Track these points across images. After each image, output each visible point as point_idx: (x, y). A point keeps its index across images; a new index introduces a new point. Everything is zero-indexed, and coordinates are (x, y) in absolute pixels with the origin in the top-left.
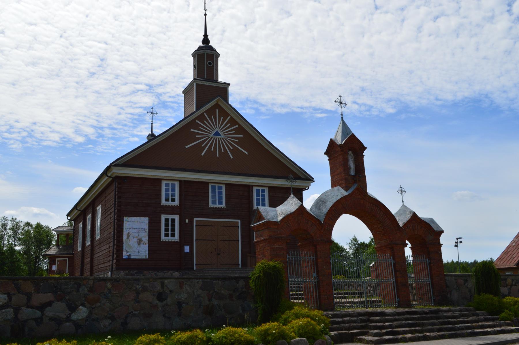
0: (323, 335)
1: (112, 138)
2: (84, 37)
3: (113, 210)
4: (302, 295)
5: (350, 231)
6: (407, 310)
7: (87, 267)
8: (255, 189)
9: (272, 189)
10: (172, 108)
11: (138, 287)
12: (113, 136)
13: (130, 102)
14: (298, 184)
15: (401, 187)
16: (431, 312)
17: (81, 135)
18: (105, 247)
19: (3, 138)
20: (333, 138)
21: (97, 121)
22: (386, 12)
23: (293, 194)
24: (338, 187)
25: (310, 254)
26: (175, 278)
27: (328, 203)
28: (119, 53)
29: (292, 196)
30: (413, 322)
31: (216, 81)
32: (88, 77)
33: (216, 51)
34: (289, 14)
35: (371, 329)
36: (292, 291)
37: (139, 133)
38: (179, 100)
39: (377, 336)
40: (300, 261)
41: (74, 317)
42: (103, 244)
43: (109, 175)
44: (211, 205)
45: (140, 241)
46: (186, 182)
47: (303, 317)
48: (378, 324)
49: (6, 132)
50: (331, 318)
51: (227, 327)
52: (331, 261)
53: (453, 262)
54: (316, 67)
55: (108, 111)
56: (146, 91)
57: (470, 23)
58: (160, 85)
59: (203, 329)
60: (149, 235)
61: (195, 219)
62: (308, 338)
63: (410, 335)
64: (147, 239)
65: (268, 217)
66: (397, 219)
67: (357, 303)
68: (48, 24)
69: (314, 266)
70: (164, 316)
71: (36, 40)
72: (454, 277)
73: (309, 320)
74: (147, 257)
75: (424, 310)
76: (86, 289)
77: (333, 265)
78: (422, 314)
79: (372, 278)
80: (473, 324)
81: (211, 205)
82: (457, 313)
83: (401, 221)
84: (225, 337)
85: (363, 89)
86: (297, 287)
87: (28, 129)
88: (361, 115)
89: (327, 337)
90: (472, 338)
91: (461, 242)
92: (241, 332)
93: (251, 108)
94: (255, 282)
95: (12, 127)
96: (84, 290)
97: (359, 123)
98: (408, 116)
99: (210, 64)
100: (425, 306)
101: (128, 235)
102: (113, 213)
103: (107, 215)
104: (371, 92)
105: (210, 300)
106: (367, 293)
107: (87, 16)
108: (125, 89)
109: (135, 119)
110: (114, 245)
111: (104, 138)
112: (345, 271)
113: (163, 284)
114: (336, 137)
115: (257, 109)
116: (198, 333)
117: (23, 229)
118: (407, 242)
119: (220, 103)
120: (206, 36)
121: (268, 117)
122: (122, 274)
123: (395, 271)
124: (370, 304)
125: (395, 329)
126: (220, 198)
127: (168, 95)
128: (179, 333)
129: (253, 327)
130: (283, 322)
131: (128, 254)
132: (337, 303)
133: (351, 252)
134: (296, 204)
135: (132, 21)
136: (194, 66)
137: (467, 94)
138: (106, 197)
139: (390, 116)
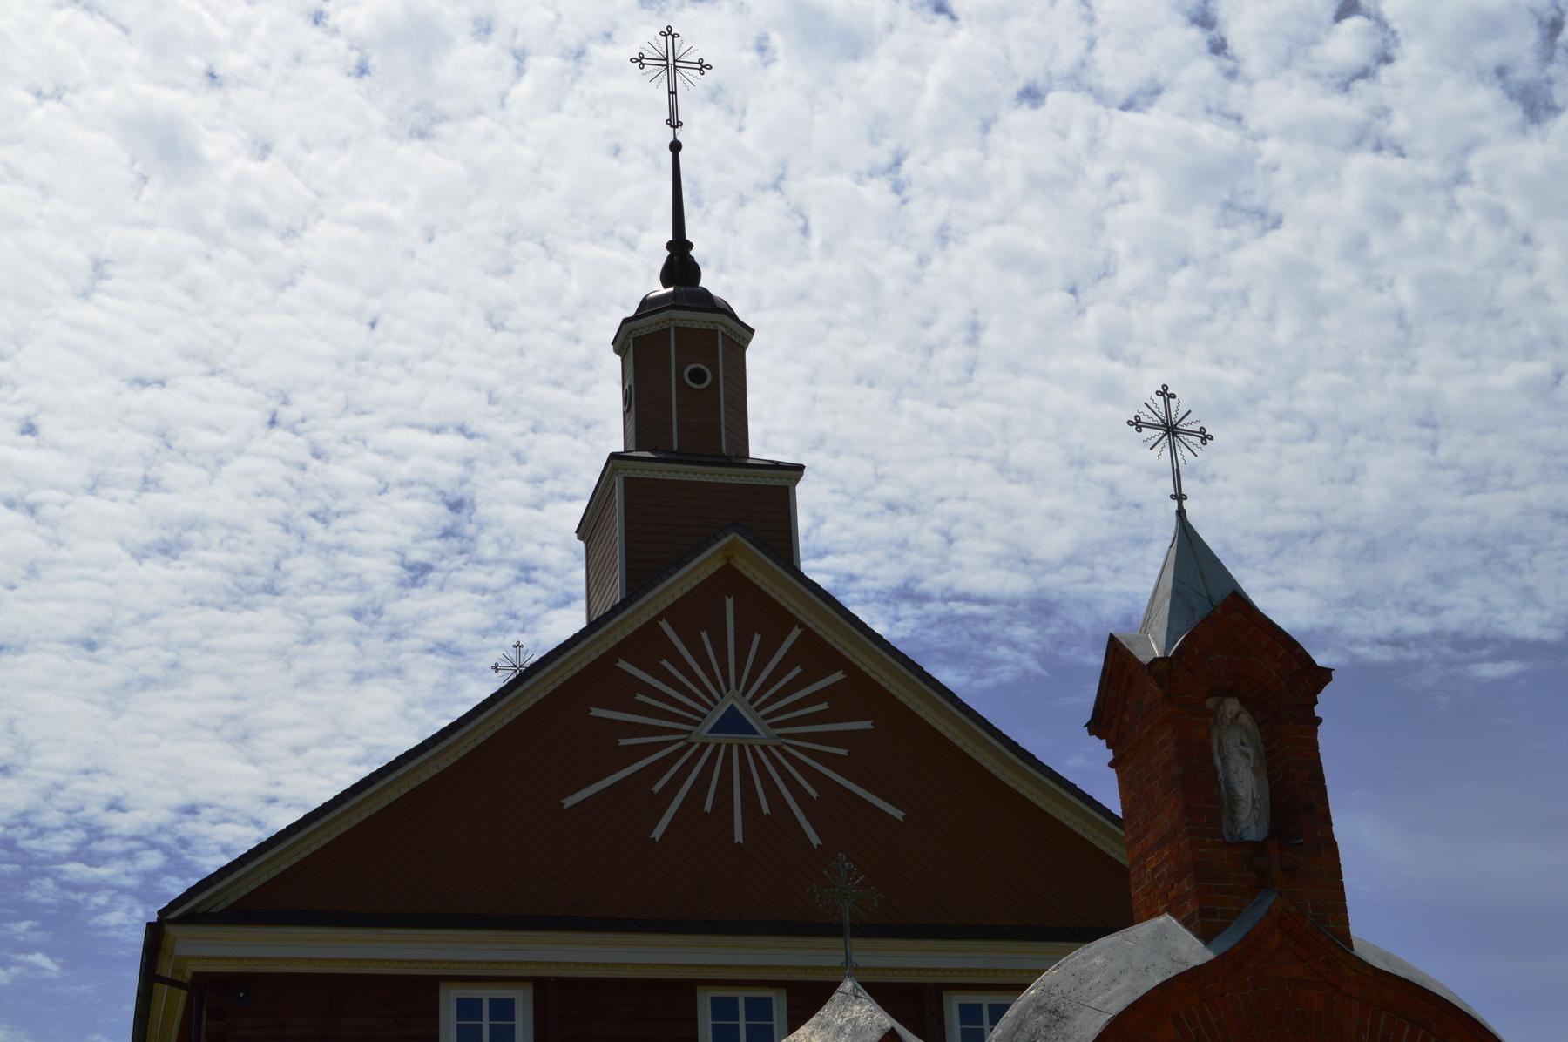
2: (363, 413)
19: (65, 886)
24: (1165, 920)
28: (525, 471)
32: (402, 584)
33: (732, 315)
34: (1270, 221)
49: (73, 857)
54: (1434, 446)
68: (213, 373)
71: (170, 447)
87: (165, 839)
95: (96, 832)
119: (742, 565)
120: (679, 246)
135: (566, 326)
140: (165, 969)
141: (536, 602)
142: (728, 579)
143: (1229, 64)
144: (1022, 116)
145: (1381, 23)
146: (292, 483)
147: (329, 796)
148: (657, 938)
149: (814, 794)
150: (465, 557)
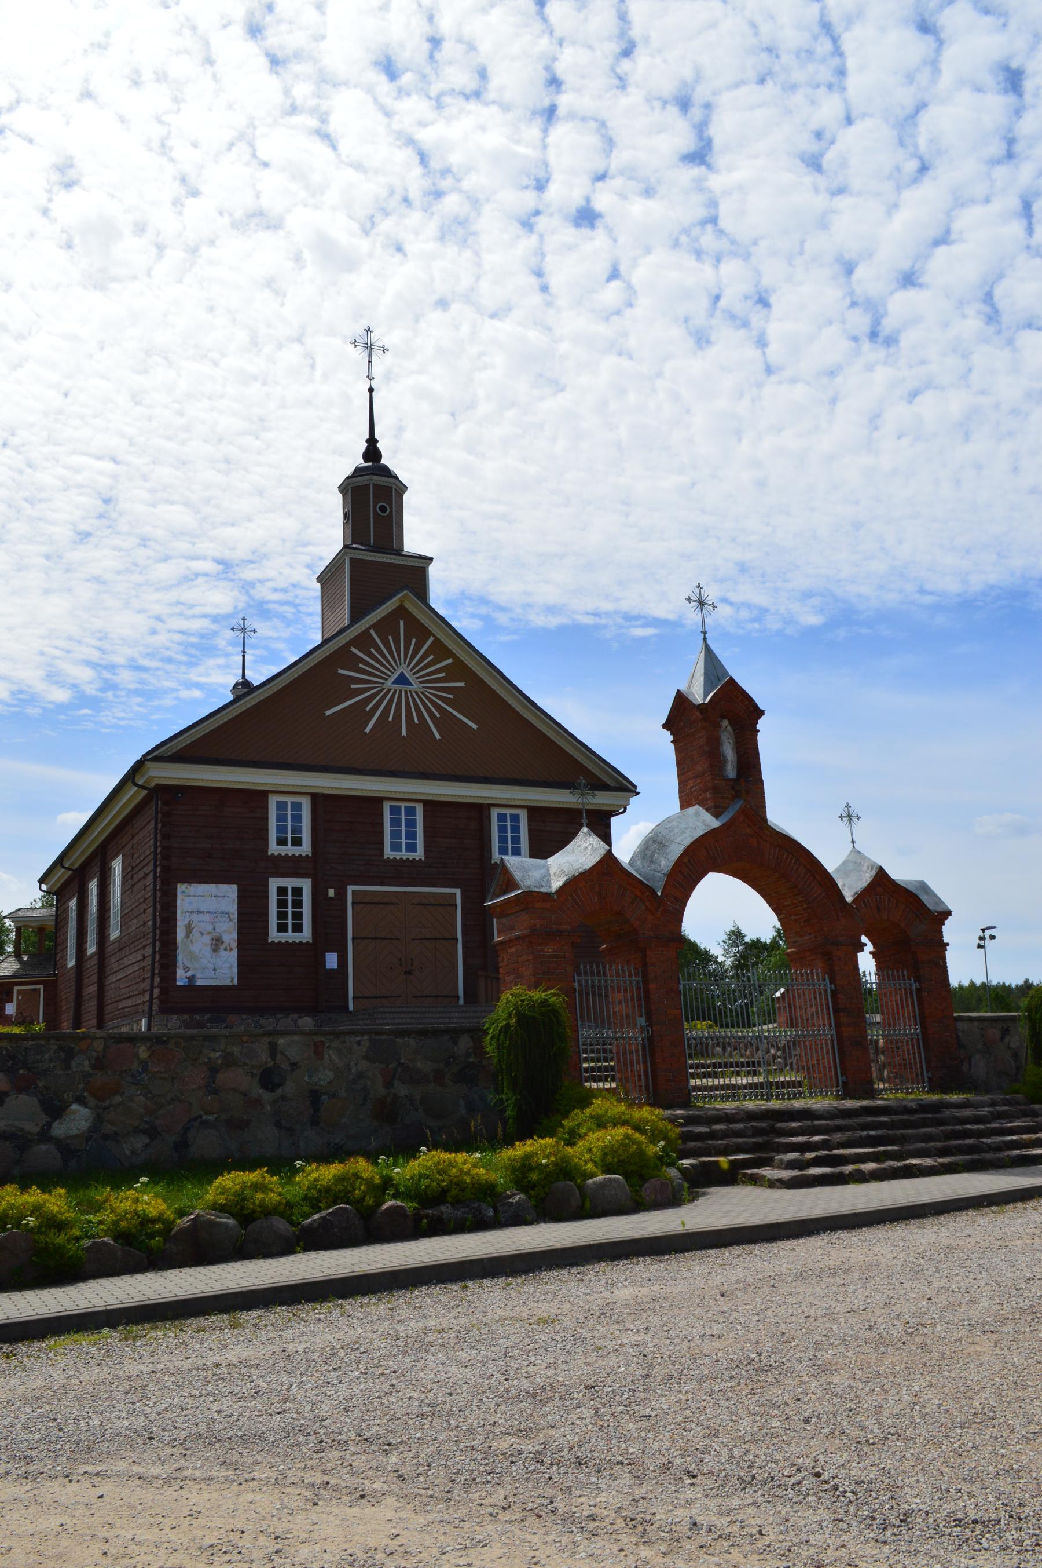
0: (664, 1168)
1: (137, 692)
2: (59, 445)
3: (151, 867)
4: (612, 1069)
5: (725, 913)
6: (865, 1103)
7: (90, 1007)
8: (495, 813)
9: (535, 812)
10: (282, 617)
11: (213, 1055)
12: (139, 686)
13: (178, 603)
14: (600, 800)
15: (848, 806)
16: (923, 1108)
17: (61, 685)
18: (132, 958)
20: (683, 688)
21: (100, 649)
22: (794, 381)
23: (588, 826)
24: (697, 807)
25: (629, 971)
26: (303, 1033)
27: (673, 847)
29: (585, 829)
30: (880, 1132)
31: (399, 551)
32: (74, 542)
33: (396, 478)
34: (558, 387)
35: (778, 1152)
36: (586, 1060)
37: (202, 680)
38: (296, 596)
39: (793, 1169)
40: (606, 987)
41: (59, 1130)
42: (127, 951)
43: (140, 783)
44: (388, 853)
45: (217, 943)
47: (615, 1125)
48: (794, 1139)
50: (681, 1125)
51: (429, 1150)
52: (681, 987)
53: (972, 984)
54: (627, 515)
55: (126, 625)
56: (218, 577)
57: (997, 406)
58: (251, 562)
59: (371, 1157)
60: (240, 929)
61: (350, 889)
62: (627, 1176)
63: (871, 1166)
64: (236, 937)
65: (528, 883)
66: (840, 885)
67: (745, 1087)
69: (639, 1000)
70: (278, 1124)
72: (976, 1024)
73: (630, 1131)
74: (236, 982)
75: (905, 1103)
76: (86, 1063)
77: (685, 995)
78: (902, 1113)
79: (780, 1026)
80: (1025, 1137)
81: (388, 853)
82: (986, 1110)
83: (849, 889)
84: (427, 1177)
85: (743, 568)
86: (598, 1051)
88: (741, 632)
89: (673, 1172)
90: (1020, 1169)
91: (992, 937)
92: (465, 1163)
93: (473, 616)
94: (498, 1039)
96: (82, 1064)
97: (736, 650)
98: (853, 633)
100: (907, 1093)
102: (151, 876)
103: (136, 879)
104: (763, 576)
105: (388, 1084)
106: (769, 1064)
107: (66, 395)
108: (164, 572)
109: (192, 645)
110: (154, 952)
111: (119, 693)
112: (714, 1009)
113: (273, 1049)
114: (690, 686)
115: (487, 619)
116: (361, 1166)
118: (864, 939)
119: (408, 605)
120: (372, 441)
121: (515, 637)
122: (174, 1023)
123: (836, 1011)
124: (775, 1091)
125: (836, 1152)
126: (411, 835)
127: (270, 584)
128: (314, 1166)
129: (494, 1150)
130: (566, 1136)
131: (189, 974)
132: (697, 1088)
133: (728, 963)
134: (594, 850)
136: (345, 516)
137: (993, 578)
138: (133, 837)
139: (811, 634)
141: (149, 558)
142: (401, 612)
143: (549, 298)
144: (437, 315)
145: (630, 287)
146: (14, 480)
147: (221, 705)
148: (368, 778)
149: (438, 715)
150: (110, 530)
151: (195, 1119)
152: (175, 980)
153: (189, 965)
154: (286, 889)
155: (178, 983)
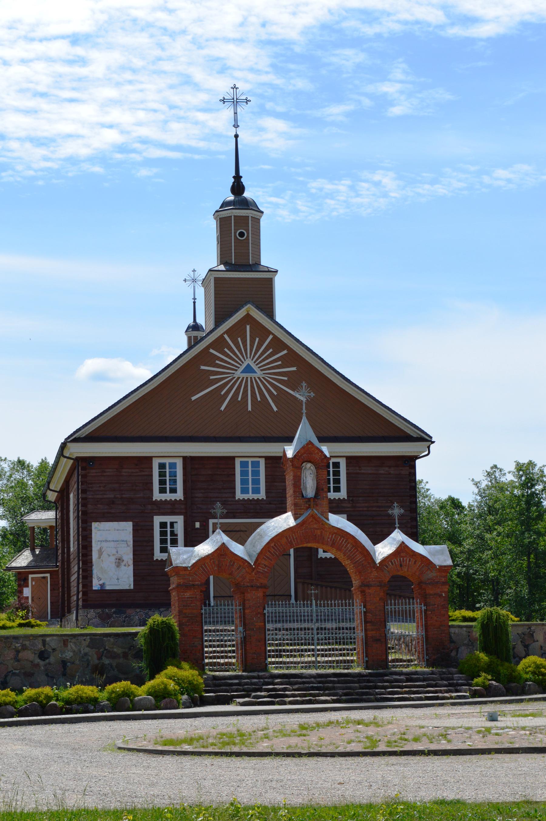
11: (17, 645)
44: (239, 495)
45: (119, 561)
46: (193, 458)
60: (134, 551)
70: (47, 675)
72: (465, 629)
74: (132, 587)
81: (239, 495)
99: (242, 235)
101: (100, 552)
105: (99, 658)
110: (79, 568)
117: (11, 476)
120: (237, 177)
123: (366, 622)
126: (256, 482)
131: (101, 582)
140: (66, 453)
142: (248, 318)
149: (275, 393)
151: (10, 672)
152: (92, 586)
153: (100, 576)
154: (166, 523)
155: (94, 588)
